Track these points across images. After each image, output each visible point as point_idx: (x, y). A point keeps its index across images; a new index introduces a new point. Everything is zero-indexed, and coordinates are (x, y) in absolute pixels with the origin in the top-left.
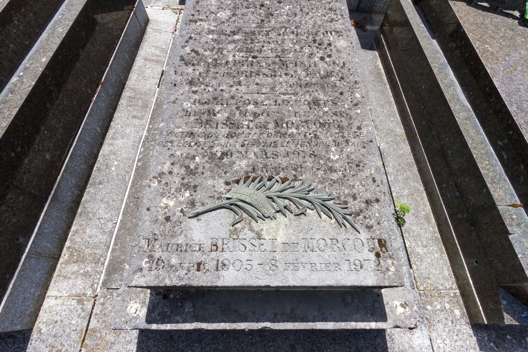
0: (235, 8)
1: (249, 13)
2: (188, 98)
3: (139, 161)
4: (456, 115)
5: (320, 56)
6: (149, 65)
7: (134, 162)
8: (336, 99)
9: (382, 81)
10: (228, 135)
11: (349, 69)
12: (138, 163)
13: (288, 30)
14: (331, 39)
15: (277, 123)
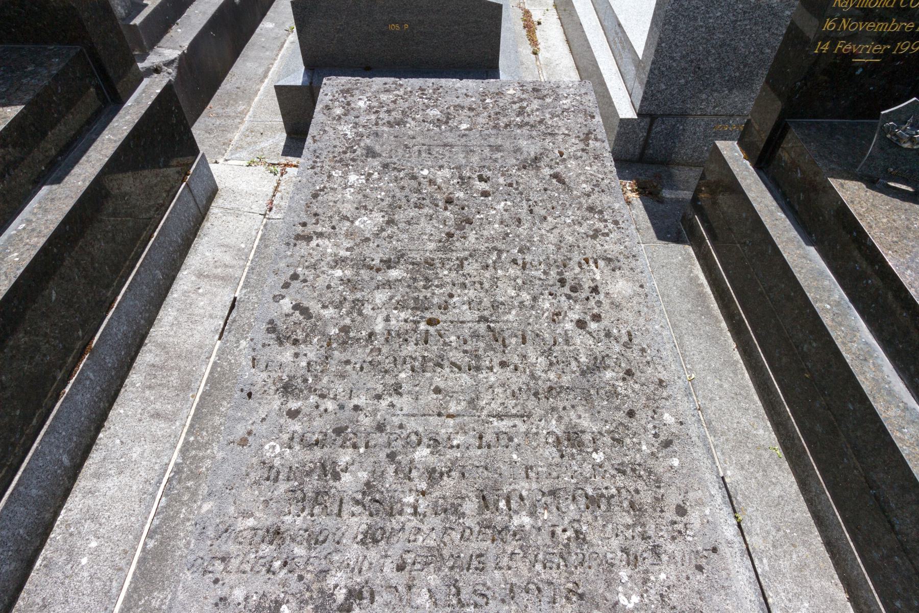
0: (394, 206)
1: (423, 219)
2: (276, 431)
3: (150, 536)
4: (895, 435)
5: (577, 317)
6: (205, 286)
7: (137, 538)
8: (621, 428)
9: (708, 312)
10: (365, 534)
11: (643, 350)
12: (148, 541)
13: (504, 255)
14: (598, 277)
15: (484, 498)
